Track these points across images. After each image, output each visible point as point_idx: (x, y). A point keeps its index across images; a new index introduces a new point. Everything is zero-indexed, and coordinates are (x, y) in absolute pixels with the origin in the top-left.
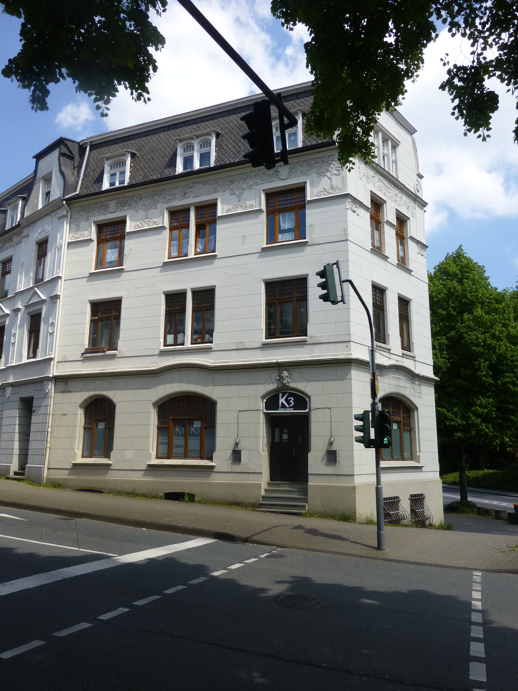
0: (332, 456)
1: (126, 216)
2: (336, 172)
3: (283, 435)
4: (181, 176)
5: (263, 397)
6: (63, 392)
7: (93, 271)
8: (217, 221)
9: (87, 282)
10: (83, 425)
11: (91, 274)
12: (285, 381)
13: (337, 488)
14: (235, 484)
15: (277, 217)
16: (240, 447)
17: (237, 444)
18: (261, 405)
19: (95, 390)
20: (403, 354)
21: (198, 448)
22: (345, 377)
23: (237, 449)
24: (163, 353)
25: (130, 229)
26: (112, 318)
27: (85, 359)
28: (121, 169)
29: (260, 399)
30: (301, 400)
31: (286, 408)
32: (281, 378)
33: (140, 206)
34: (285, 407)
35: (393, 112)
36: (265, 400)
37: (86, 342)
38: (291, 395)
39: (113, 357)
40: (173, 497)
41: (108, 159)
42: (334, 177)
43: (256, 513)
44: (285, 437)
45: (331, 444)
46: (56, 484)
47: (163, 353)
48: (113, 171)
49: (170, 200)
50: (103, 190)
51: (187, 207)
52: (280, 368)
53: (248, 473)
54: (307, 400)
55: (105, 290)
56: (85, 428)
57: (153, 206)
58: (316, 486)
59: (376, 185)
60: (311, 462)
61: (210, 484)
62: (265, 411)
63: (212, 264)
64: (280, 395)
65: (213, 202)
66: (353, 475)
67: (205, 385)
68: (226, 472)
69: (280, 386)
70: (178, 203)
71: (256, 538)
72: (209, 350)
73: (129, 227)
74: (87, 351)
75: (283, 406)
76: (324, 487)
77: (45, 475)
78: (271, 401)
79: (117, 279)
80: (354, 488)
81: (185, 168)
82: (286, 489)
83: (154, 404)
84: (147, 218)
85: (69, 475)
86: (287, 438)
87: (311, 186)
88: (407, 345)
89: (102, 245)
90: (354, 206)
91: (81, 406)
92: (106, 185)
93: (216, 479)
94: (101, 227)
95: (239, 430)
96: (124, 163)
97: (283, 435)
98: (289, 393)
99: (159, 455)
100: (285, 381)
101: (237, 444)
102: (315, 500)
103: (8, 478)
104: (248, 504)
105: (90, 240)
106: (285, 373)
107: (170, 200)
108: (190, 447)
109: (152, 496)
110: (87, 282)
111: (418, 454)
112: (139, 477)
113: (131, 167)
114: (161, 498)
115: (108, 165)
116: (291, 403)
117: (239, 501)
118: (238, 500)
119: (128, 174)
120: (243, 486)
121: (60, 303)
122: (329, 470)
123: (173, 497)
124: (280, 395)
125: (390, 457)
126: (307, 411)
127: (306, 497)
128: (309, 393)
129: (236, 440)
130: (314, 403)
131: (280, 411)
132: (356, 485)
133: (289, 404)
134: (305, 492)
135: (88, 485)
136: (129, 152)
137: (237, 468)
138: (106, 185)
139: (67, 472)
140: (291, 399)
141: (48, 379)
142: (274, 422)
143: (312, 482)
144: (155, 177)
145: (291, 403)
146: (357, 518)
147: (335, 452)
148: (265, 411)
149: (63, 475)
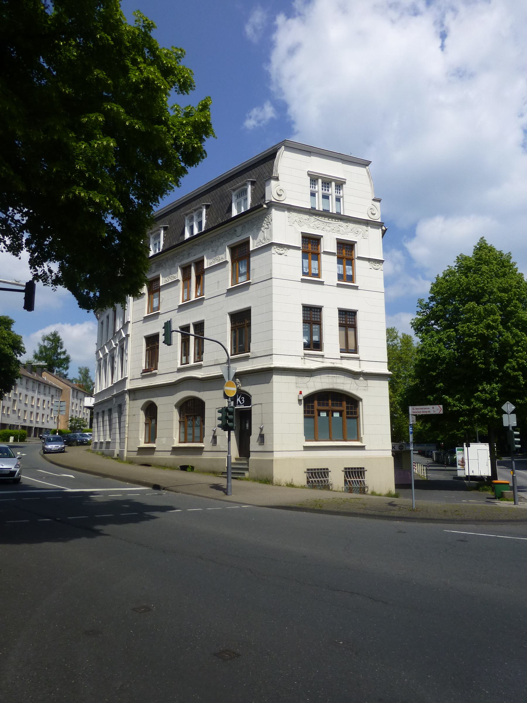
0: (262, 438)
1: (204, 256)
2: (267, 226)
4: (189, 239)
6: (133, 400)
7: (230, 287)
8: (205, 273)
9: (178, 312)
10: (144, 421)
11: (229, 290)
15: (238, 264)
17: (261, 429)
19: (148, 398)
20: (341, 357)
21: (199, 435)
22: (268, 381)
24: (179, 370)
25: (207, 265)
26: (246, 325)
27: (143, 377)
28: (244, 197)
33: (167, 266)
37: (144, 365)
39: (155, 375)
40: (184, 468)
41: (234, 190)
42: (265, 231)
43: (219, 478)
46: (131, 462)
47: (179, 370)
48: (155, 242)
49: (182, 260)
50: (233, 216)
51: (189, 264)
55: (238, 303)
56: (180, 422)
57: (173, 266)
59: (311, 225)
60: (251, 443)
61: (201, 459)
63: (158, 318)
65: (246, 240)
66: (273, 452)
67: (199, 391)
70: (186, 261)
71: (174, 488)
72: (247, 358)
73: (162, 282)
74: (145, 371)
75: (239, 404)
77: (125, 455)
79: (157, 320)
80: (272, 460)
81: (199, 230)
83: (176, 406)
84: (170, 274)
85: (137, 455)
87: (253, 239)
88: (349, 348)
89: (151, 296)
90: (281, 249)
91: (142, 409)
92: (235, 213)
93: (205, 456)
94: (233, 250)
96: (245, 191)
99: (181, 441)
103: (113, 458)
105: (226, 262)
107: (182, 259)
108: (195, 435)
109: (172, 468)
110: (178, 312)
111: (362, 436)
112: (168, 456)
113: (164, 236)
114: (178, 469)
115: (235, 196)
119: (162, 243)
121: (130, 339)
122: (260, 448)
123: (184, 468)
125: (342, 439)
128: (204, 399)
132: (274, 458)
133: (242, 402)
135: (145, 462)
136: (249, 181)
138: (235, 213)
139: (136, 453)
141: (124, 392)
143: (253, 457)
144: (174, 244)
146: (274, 482)
149: (134, 455)
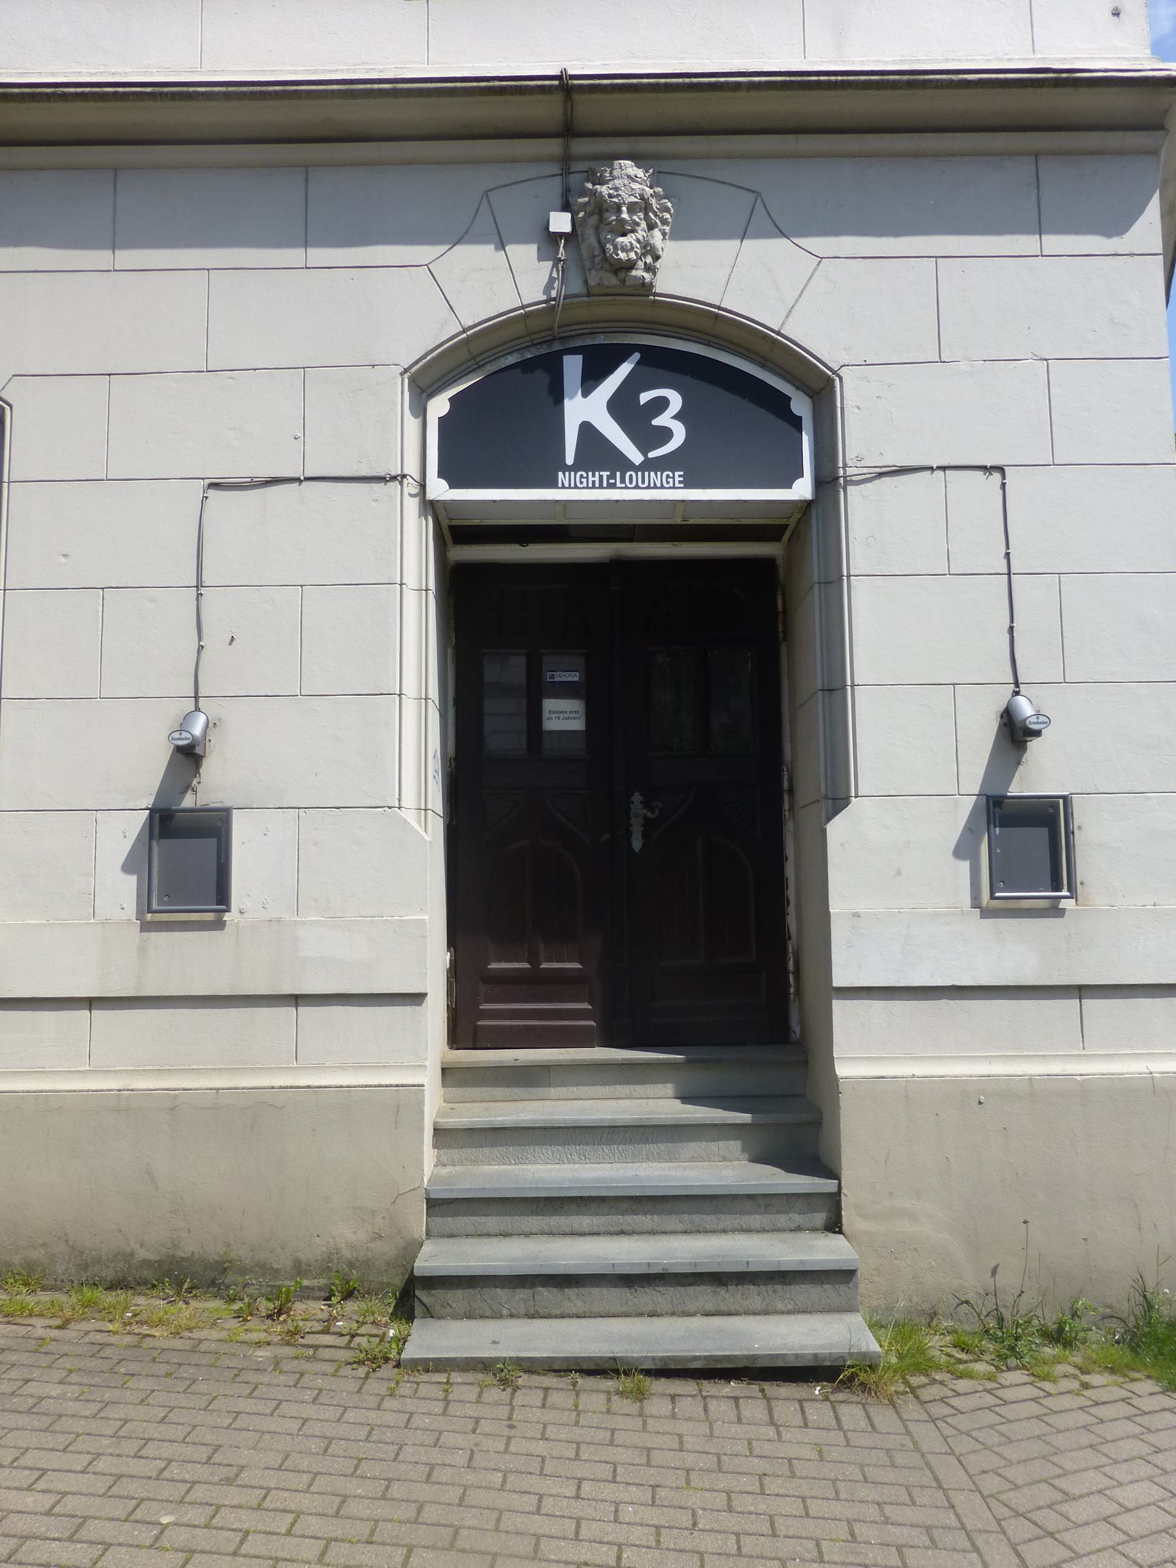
3: (550, 705)
5: (423, 382)
12: (626, 246)
13: (1083, 1093)
14: (173, 1106)
16: (213, 786)
17: (188, 757)
18: (409, 440)
23: (188, 802)
29: (400, 393)
30: (757, 391)
31: (622, 468)
32: (600, 218)
34: (615, 462)
35: (551, 159)
36: (439, 406)
38: (661, 364)
44: (563, 716)
45: (1015, 734)
52: (581, 146)
53: (297, 1000)
54: (800, 406)
58: (909, 1093)
62: (439, 489)
64: (573, 366)
68: (90, 1003)
69: (576, 287)
75: (596, 453)
76: (974, 1097)
78: (496, 396)
82: (625, 1116)
86: (577, 724)
95: (214, 639)
97: (550, 705)
98: (644, 349)
100: (626, 246)
101: (188, 757)
102: (903, 1205)
104: (300, 1270)
106: (628, 180)
116: (665, 434)
117: (214, 1251)
118: (200, 1241)
120: (251, 1118)
122: (1013, 950)
124: (573, 366)
126: (802, 489)
127: (829, 1185)
129: (187, 718)
130: (868, 427)
131: (576, 491)
134: (799, 1129)
137: (190, 959)
140: (661, 405)
142: (502, 607)
143: (864, 1052)
145: (665, 434)
147: (213, 828)
148: (439, 489)
